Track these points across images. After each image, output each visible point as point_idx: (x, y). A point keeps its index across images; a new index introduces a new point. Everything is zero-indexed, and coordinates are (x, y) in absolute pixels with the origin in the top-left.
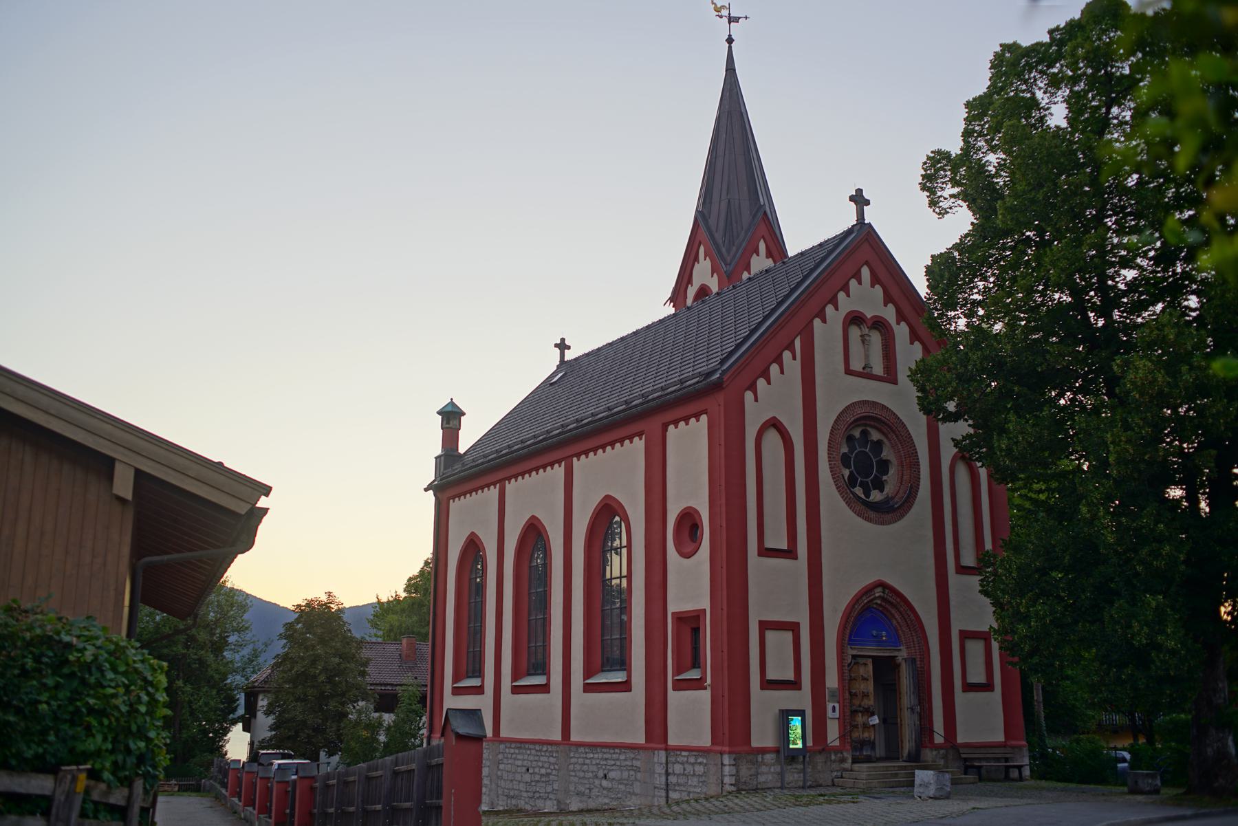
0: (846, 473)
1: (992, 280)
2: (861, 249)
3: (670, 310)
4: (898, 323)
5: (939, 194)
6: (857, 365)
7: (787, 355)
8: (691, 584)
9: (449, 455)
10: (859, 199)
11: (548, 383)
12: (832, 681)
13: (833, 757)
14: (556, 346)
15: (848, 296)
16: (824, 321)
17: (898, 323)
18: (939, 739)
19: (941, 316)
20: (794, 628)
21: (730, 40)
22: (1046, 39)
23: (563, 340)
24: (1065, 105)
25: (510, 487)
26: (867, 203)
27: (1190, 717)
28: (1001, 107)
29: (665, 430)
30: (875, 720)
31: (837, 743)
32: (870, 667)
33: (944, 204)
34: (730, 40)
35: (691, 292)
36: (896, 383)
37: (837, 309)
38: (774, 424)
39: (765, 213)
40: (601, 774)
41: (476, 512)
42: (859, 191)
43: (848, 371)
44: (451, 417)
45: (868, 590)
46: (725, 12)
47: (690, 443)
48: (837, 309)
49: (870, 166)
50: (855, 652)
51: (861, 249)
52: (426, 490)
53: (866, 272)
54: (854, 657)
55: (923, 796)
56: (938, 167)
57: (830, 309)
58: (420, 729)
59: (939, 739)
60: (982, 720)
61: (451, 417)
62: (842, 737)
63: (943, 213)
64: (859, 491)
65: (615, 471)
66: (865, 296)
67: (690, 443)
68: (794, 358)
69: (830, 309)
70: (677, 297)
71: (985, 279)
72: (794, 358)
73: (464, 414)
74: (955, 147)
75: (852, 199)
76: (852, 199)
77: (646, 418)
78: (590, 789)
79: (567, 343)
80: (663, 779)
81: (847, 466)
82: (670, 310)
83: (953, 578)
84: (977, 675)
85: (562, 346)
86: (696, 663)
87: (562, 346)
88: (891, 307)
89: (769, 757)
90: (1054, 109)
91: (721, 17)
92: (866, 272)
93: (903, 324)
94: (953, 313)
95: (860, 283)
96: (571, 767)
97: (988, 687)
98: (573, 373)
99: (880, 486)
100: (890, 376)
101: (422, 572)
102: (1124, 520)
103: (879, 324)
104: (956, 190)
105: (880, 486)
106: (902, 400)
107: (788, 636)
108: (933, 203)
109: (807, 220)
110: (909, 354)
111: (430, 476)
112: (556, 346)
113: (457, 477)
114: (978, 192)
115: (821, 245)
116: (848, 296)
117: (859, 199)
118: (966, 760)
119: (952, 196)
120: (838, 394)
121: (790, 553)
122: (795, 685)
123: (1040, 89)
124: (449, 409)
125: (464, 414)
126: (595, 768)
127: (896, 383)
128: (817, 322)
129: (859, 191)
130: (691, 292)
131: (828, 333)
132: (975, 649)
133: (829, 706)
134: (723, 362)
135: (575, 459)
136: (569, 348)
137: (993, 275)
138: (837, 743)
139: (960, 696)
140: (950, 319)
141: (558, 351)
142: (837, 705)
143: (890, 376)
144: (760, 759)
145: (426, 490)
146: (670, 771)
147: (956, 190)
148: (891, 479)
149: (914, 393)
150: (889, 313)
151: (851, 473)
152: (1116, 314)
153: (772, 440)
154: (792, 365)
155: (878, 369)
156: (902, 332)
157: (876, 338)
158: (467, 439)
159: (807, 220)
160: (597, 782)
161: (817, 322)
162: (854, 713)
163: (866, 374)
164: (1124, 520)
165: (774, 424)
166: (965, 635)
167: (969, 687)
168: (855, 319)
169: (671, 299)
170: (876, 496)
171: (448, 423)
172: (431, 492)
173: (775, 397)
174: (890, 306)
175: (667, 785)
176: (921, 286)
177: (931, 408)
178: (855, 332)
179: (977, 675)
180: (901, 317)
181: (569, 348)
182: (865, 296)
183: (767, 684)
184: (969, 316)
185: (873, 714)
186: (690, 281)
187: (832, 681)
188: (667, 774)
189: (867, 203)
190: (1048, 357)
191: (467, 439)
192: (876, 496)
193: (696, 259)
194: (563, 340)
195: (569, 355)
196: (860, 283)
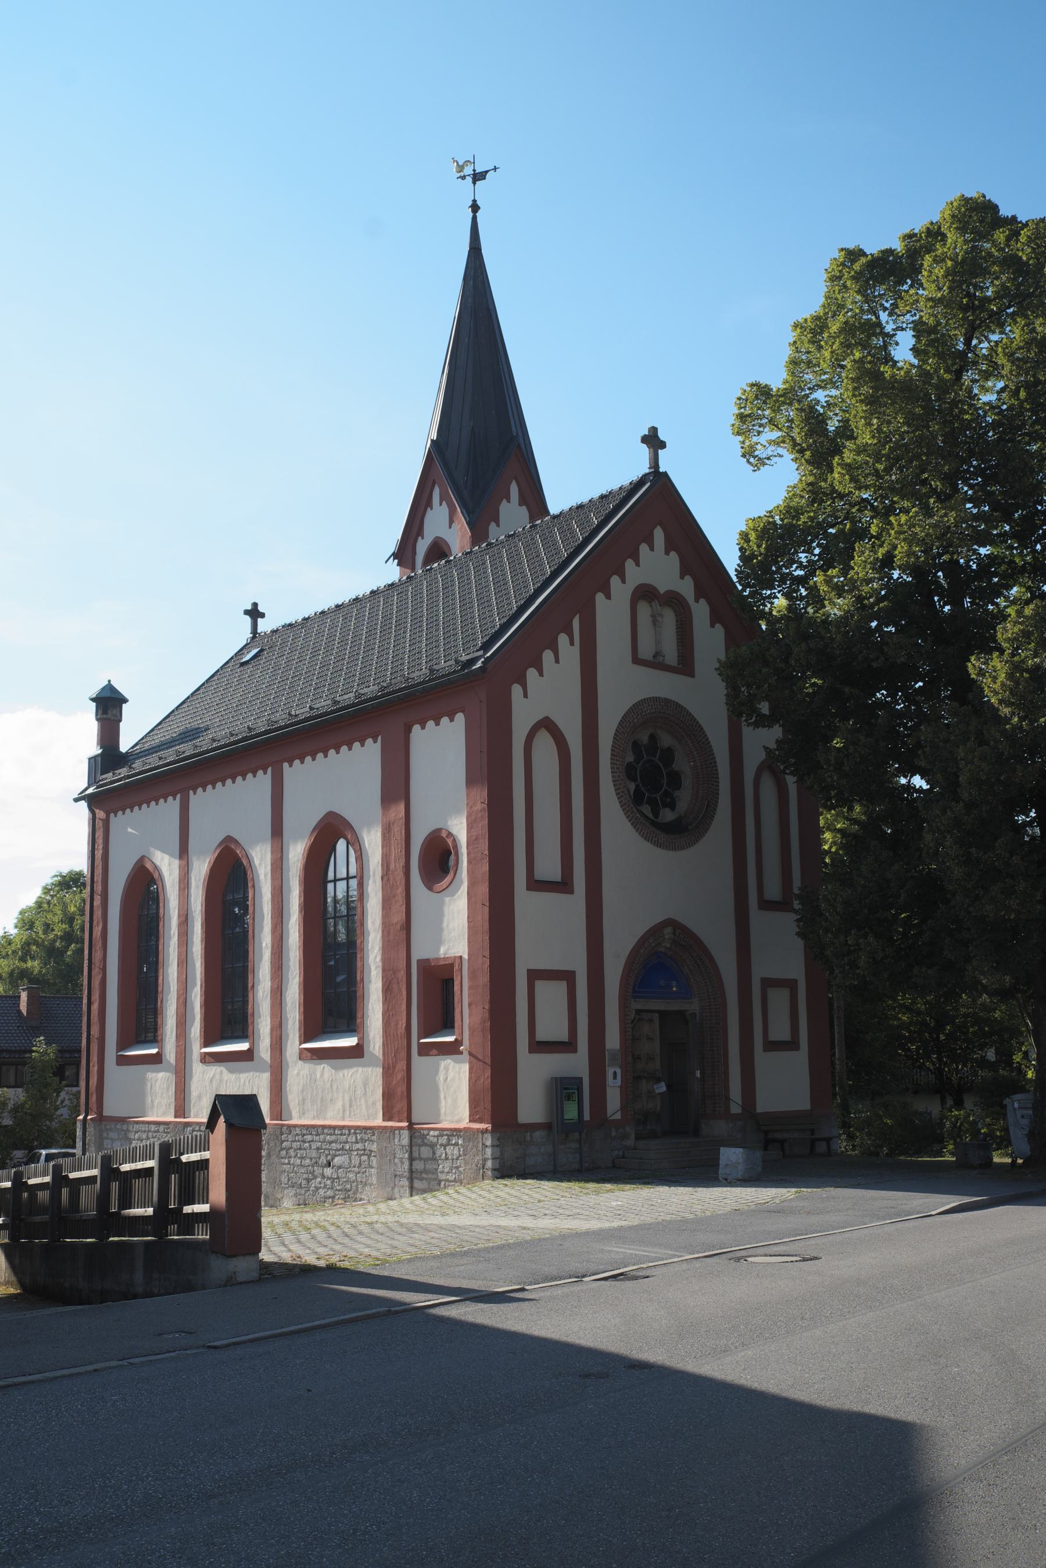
0: (632, 786)
1: (817, 551)
2: (654, 507)
3: (393, 573)
4: (697, 601)
5: (755, 439)
6: (646, 651)
7: (563, 639)
8: (452, 924)
9: (109, 757)
10: (653, 441)
11: (236, 663)
12: (613, 1040)
13: (614, 1134)
14: (247, 612)
15: (638, 565)
16: (608, 596)
17: (697, 601)
18: (735, 1109)
19: (752, 595)
20: (568, 977)
21: (475, 207)
22: (898, 246)
23: (255, 605)
24: (912, 333)
25: (199, 800)
26: (663, 445)
27: (150, 1211)
28: (842, 332)
29: (408, 730)
30: (662, 1088)
31: (618, 1116)
32: (657, 1024)
33: (760, 452)
34: (475, 207)
35: (422, 547)
36: (692, 675)
37: (624, 581)
38: (547, 724)
39: (519, 446)
40: (323, 1160)
41: (148, 835)
42: (654, 430)
43: (636, 660)
44: (109, 704)
45: (655, 932)
46: (468, 170)
47: (441, 748)
48: (624, 581)
49: (670, 395)
50: (639, 1006)
51: (654, 507)
52: (76, 800)
53: (659, 534)
54: (638, 1012)
55: (730, 1178)
56: (759, 404)
57: (615, 580)
58: (57, 1109)
59: (735, 1109)
60: (784, 1083)
61: (109, 704)
62: (623, 1108)
63: (761, 462)
64: (646, 809)
65: (343, 779)
66: (657, 565)
67: (441, 748)
68: (572, 643)
69: (615, 580)
70: (403, 554)
71: (809, 551)
72: (572, 643)
73: (125, 701)
74: (777, 379)
75: (645, 440)
76: (645, 440)
77: (384, 716)
78: (308, 1180)
79: (261, 609)
80: (406, 1166)
81: (633, 779)
82: (393, 573)
83: (758, 918)
84: (780, 1031)
85: (254, 613)
86: (447, 1024)
87: (254, 613)
88: (688, 579)
89: (538, 1135)
90: (900, 336)
91: (463, 178)
92: (659, 534)
93: (702, 601)
94: (769, 592)
95: (652, 549)
96: (284, 1153)
97: (792, 1045)
98: (267, 650)
99: (672, 806)
100: (685, 666)
101: (39, 904)
102: (973, 850)
103: (673, 600)
104: (776, 434)
105: (672, 806)
106: (705, 698)
107: (562, 986)
108: (749, 453)
109: (577, 464)
110: (710, 642)
111: (79, 780)
112: (247, 612)
113: (119, 783)
114: (819, 445)
115: (602, 497)
116: (638, 565)
117: (653, 441)
118: (766, 1132)
119: (770, 442)
120: (623, 688)
121: (564, 886)
122: (568, 1046)
123: (885, 309)
124: (108, 694)
125: (125, 701)
126: (314, 1154)
127: (692, 675)
128: (600, 597)
129: (654, 430)
130: (422, 547)
131: (612, 612)
132: (779, 999)
133: (610, 1072)
134: (486, 647)
135: (286, 765)
136: (263, 615)
137: (819, 545)
138: (618, 1116)
139: (761, 1057)
140: (764, 599)
141: (248, 619)
142: (619, 1071)
143: (685, 666)
144: (528, 1138)
145: (76, 800)
146: (415, 1154)
147: (776, 434)
148: (684, 798)
149: (719, 689)
150: (686, 588)
151: (637, 786)
152: (967, 602)
153: (544, 743)
154: (569, 651)
155: (671, 656)
156: (701, 611)
157: (669, 619)
158: (130, 735)
159: (577, 464)
160: (318, 1171)
161: (600, 597)
162: (637, 1079)
163: (656, 663)
164: (973, 850)
165: (547, 724)
166: (768, 983)
167: (771, 1046)
168: (645, 593)
169: (395, 555)
170: (668, 816)
171: (105, 712)
172: (83, 804)
173: (548, 693)
174: (688, 578)
175: (411, 1171)
176: (730, 560)
177: (740, 710)
178: (644, 610)
179: (780, 1031)
180: (700, 593)
181: (263, 615)
182: (657, 565)
183: (538, 1046)
184: (787, 596)
185: (658, 1080)
186: (420, 533)
187: (613, 1040)
188: (411, 1159)
189: (663, 445)
190: (886, 649)
191: (130, 735)
192: (668, 816)
193: (429, 504)
194: (255, 605)
195: (265, 626)
196: (652, 549)
